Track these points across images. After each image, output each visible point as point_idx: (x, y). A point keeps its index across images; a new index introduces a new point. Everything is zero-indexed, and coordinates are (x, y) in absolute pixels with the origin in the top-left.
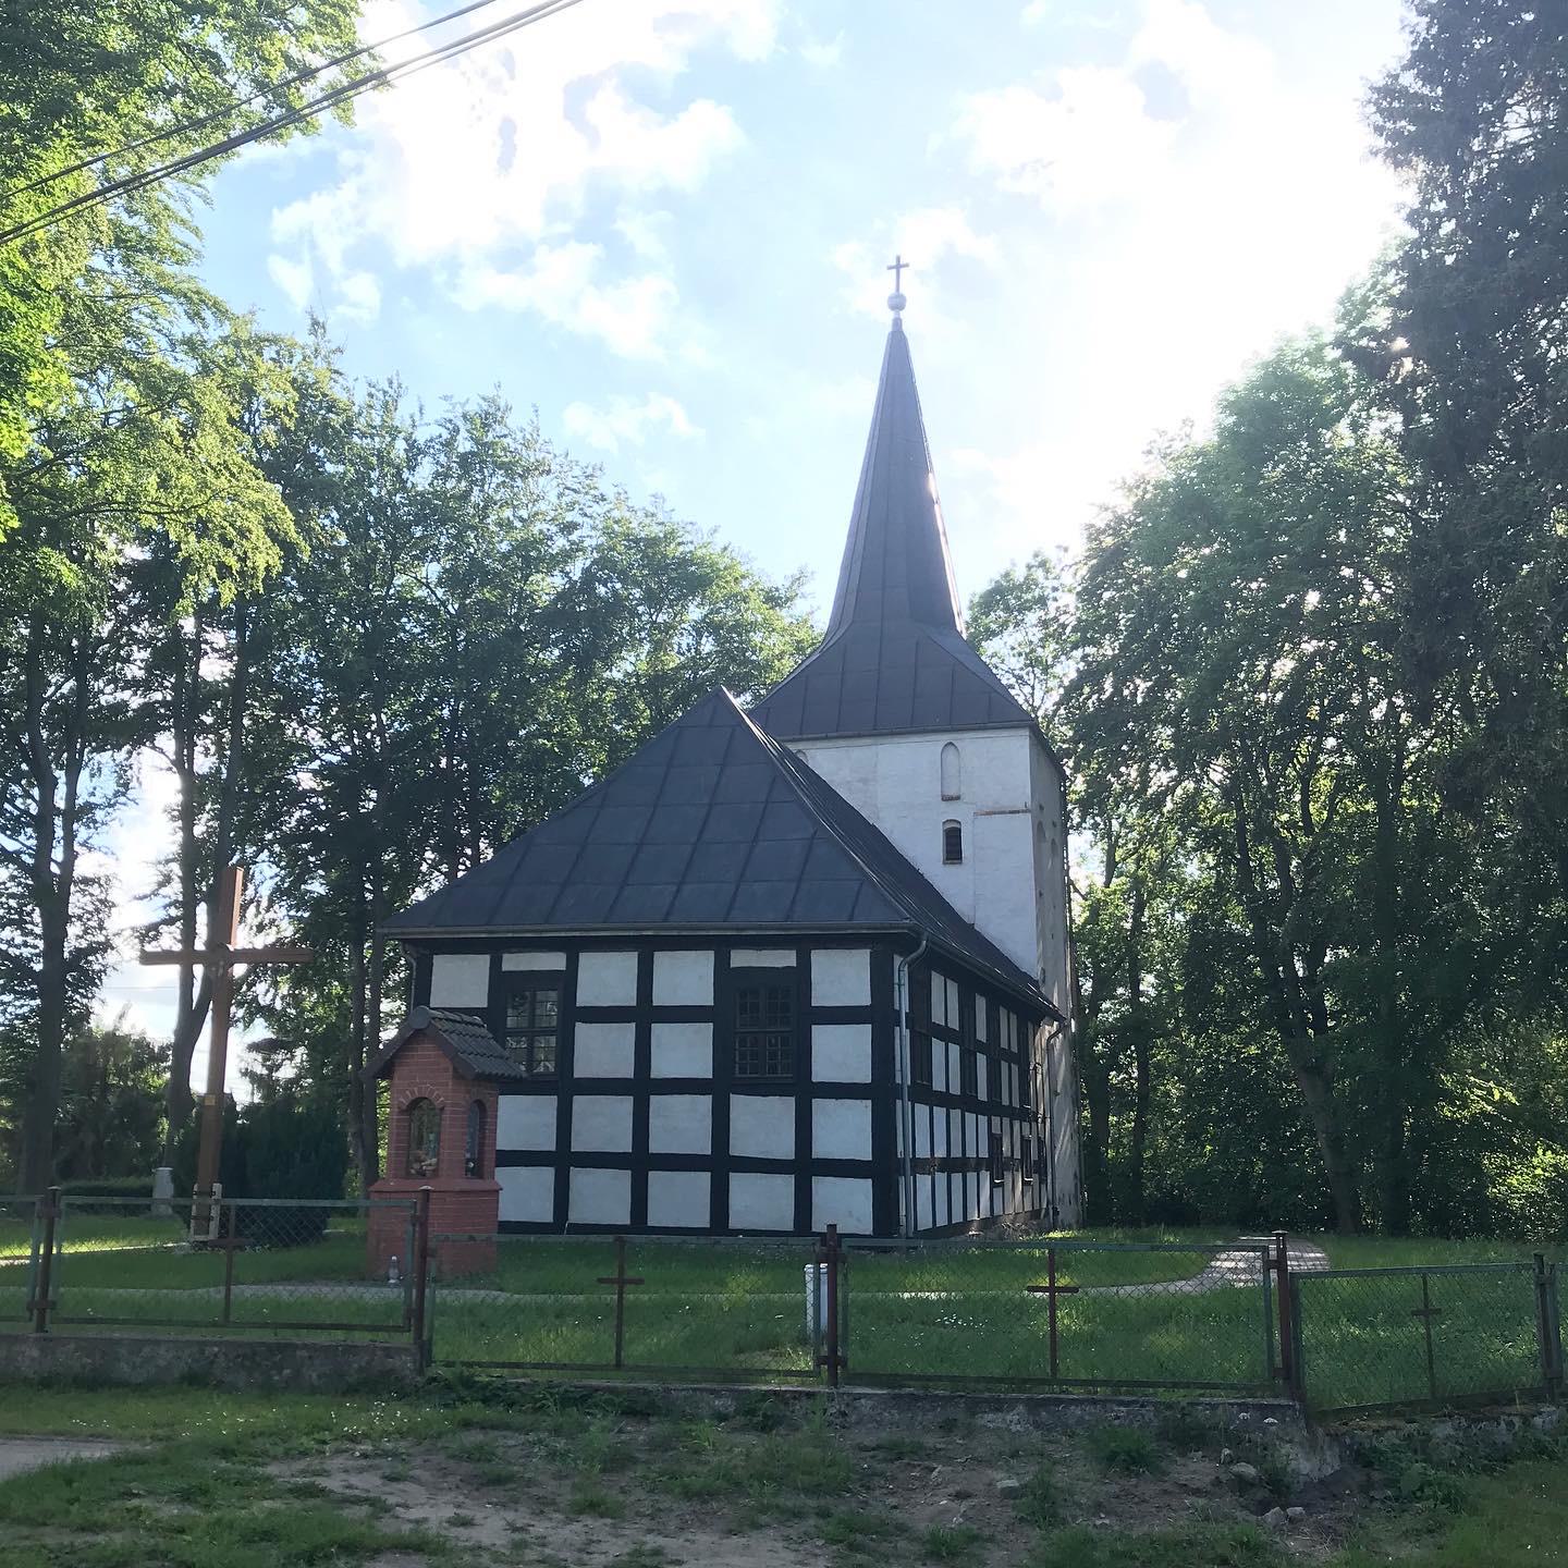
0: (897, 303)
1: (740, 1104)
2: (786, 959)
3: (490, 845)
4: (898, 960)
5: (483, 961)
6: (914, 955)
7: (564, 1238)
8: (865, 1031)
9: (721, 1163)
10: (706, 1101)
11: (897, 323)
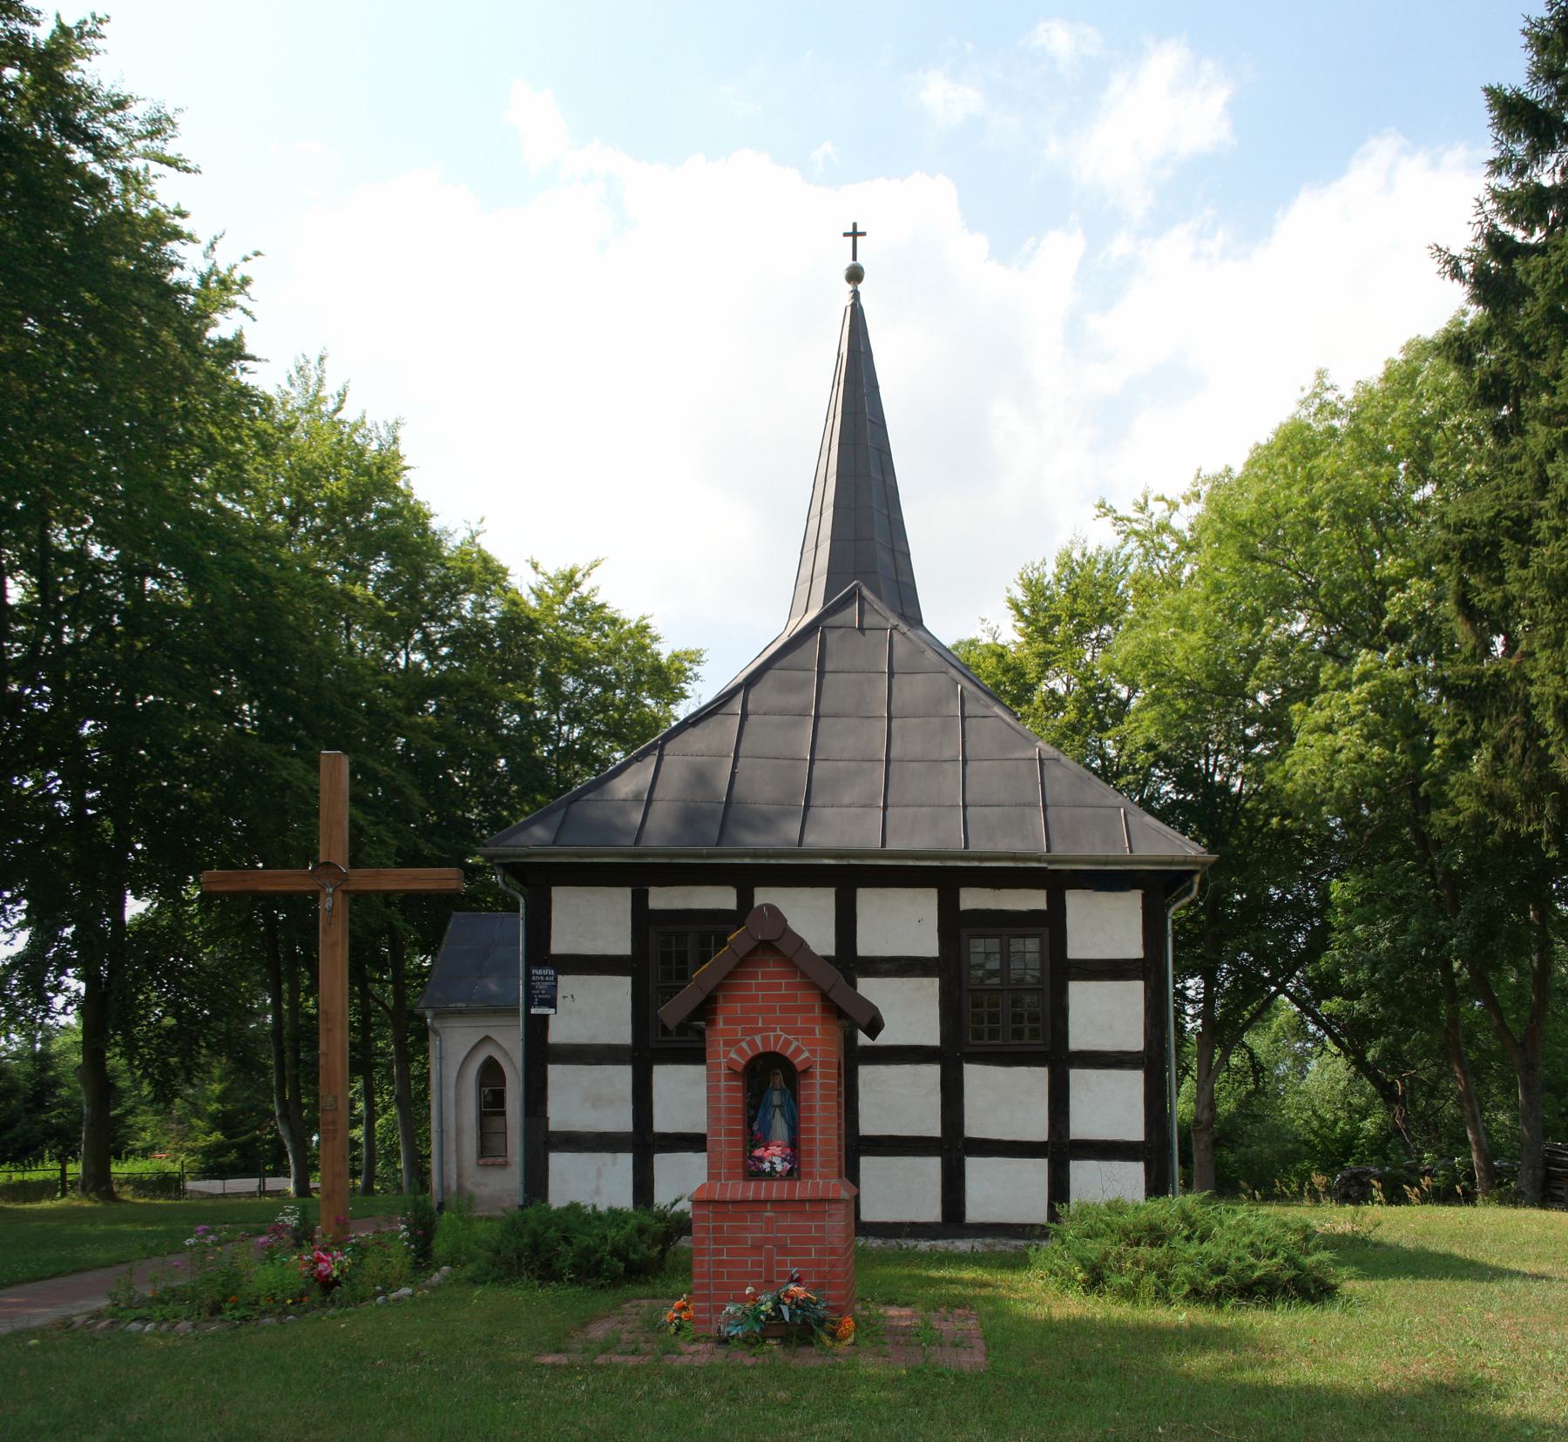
0: (855, 275)
10: (932, 1072)
11: (856, 295)
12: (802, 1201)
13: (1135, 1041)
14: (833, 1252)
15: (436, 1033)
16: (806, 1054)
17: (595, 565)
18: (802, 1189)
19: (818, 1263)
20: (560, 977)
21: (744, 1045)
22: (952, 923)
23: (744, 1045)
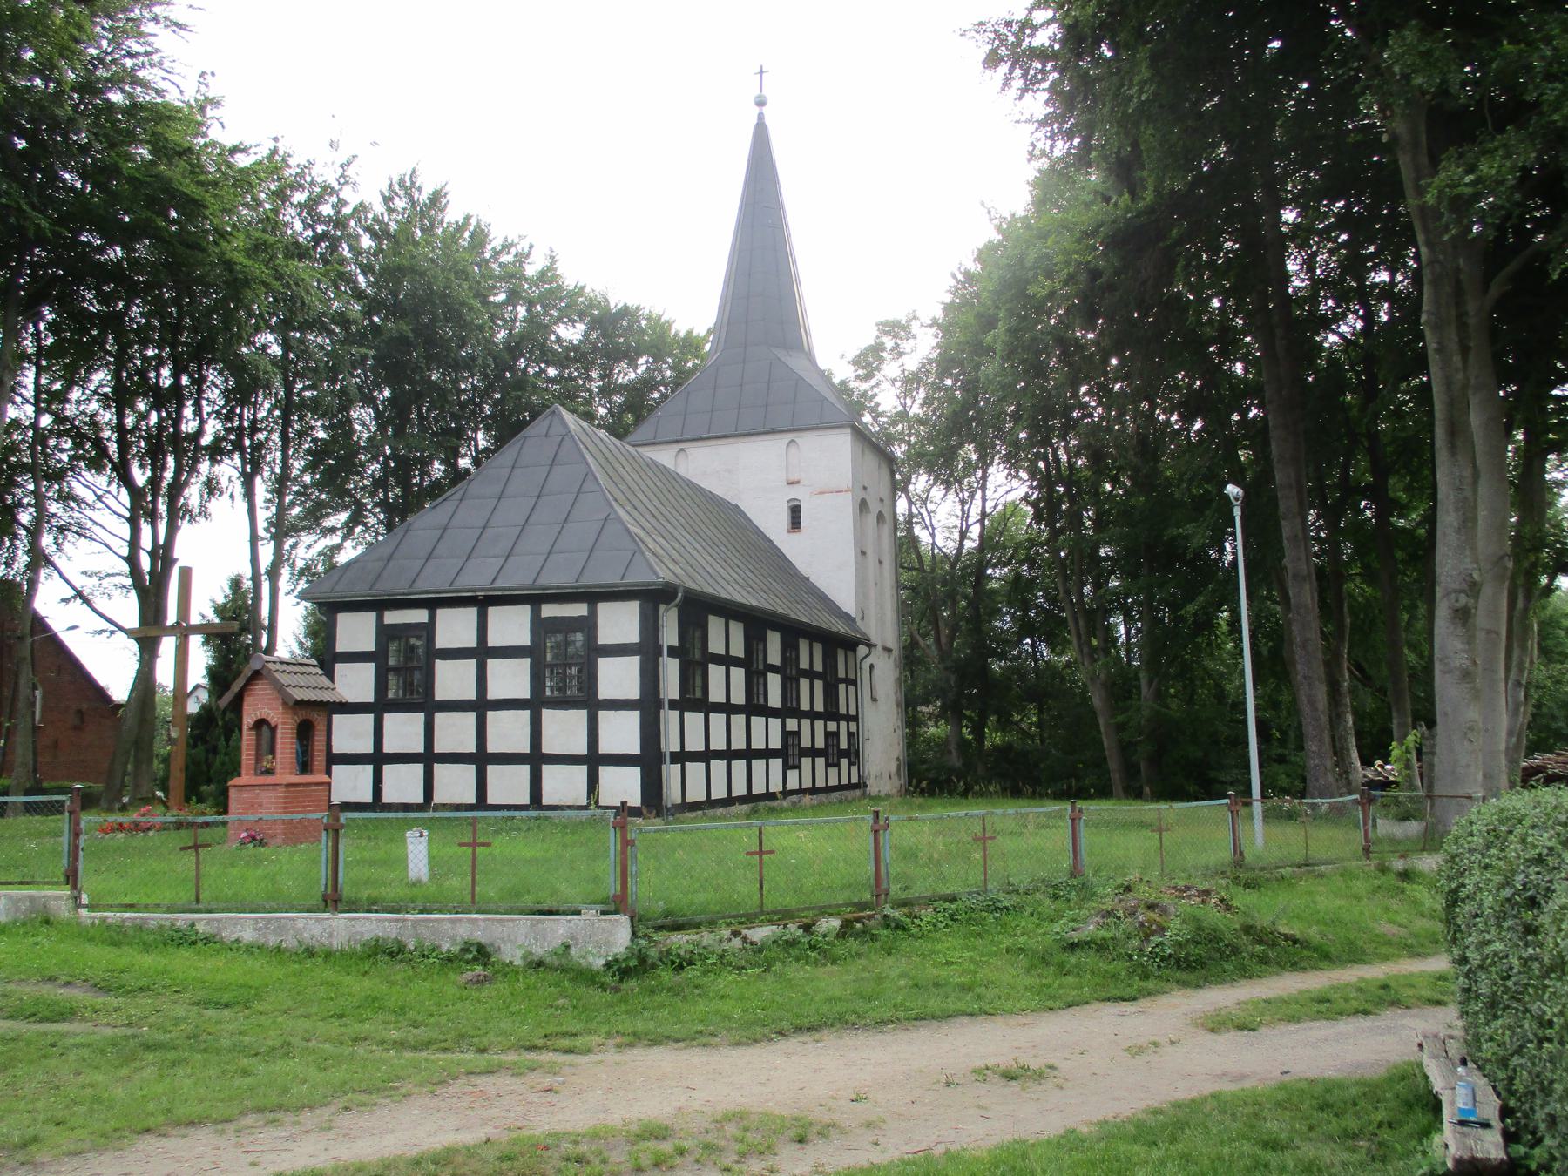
3: (1285, 278)
5: (371, 617)
7: (430, 814)
9: (536, 759)
10: (525, 715)
11: (761, 117)
13: (634, 693)
22: (540, 627)
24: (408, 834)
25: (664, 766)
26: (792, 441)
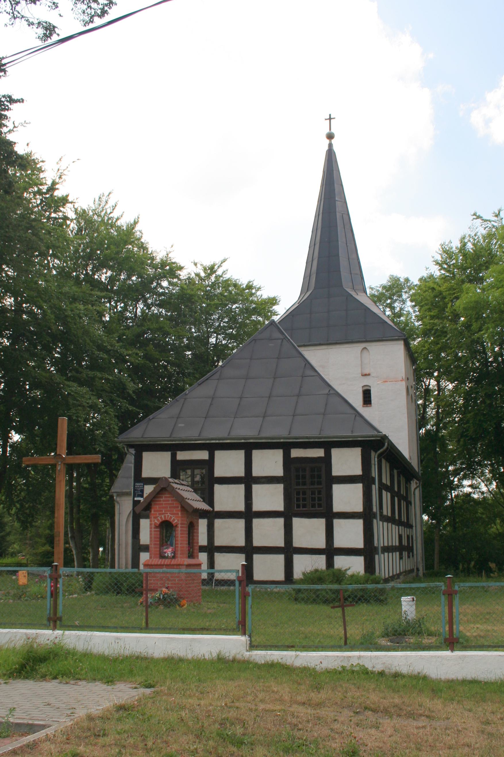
1: (297, 522)
2: (319, 453)
4: (373, 454)
5: (167, 456)
6: (381, 450)
8: (359, 487)
10: (281, 521)
11: (330, 145)
12: (174, 565)
13: (359, 508)
14: (182, 580)
15: (118, 503)
16: (176, 521)
17: (224, 261)
18: (174, 562)
19: (178, 584)
20: (145, 486)
21: (159, 518)
23: (159, 518)
24: (403, 599)
25: (377, 557)
26: (365, 348)
